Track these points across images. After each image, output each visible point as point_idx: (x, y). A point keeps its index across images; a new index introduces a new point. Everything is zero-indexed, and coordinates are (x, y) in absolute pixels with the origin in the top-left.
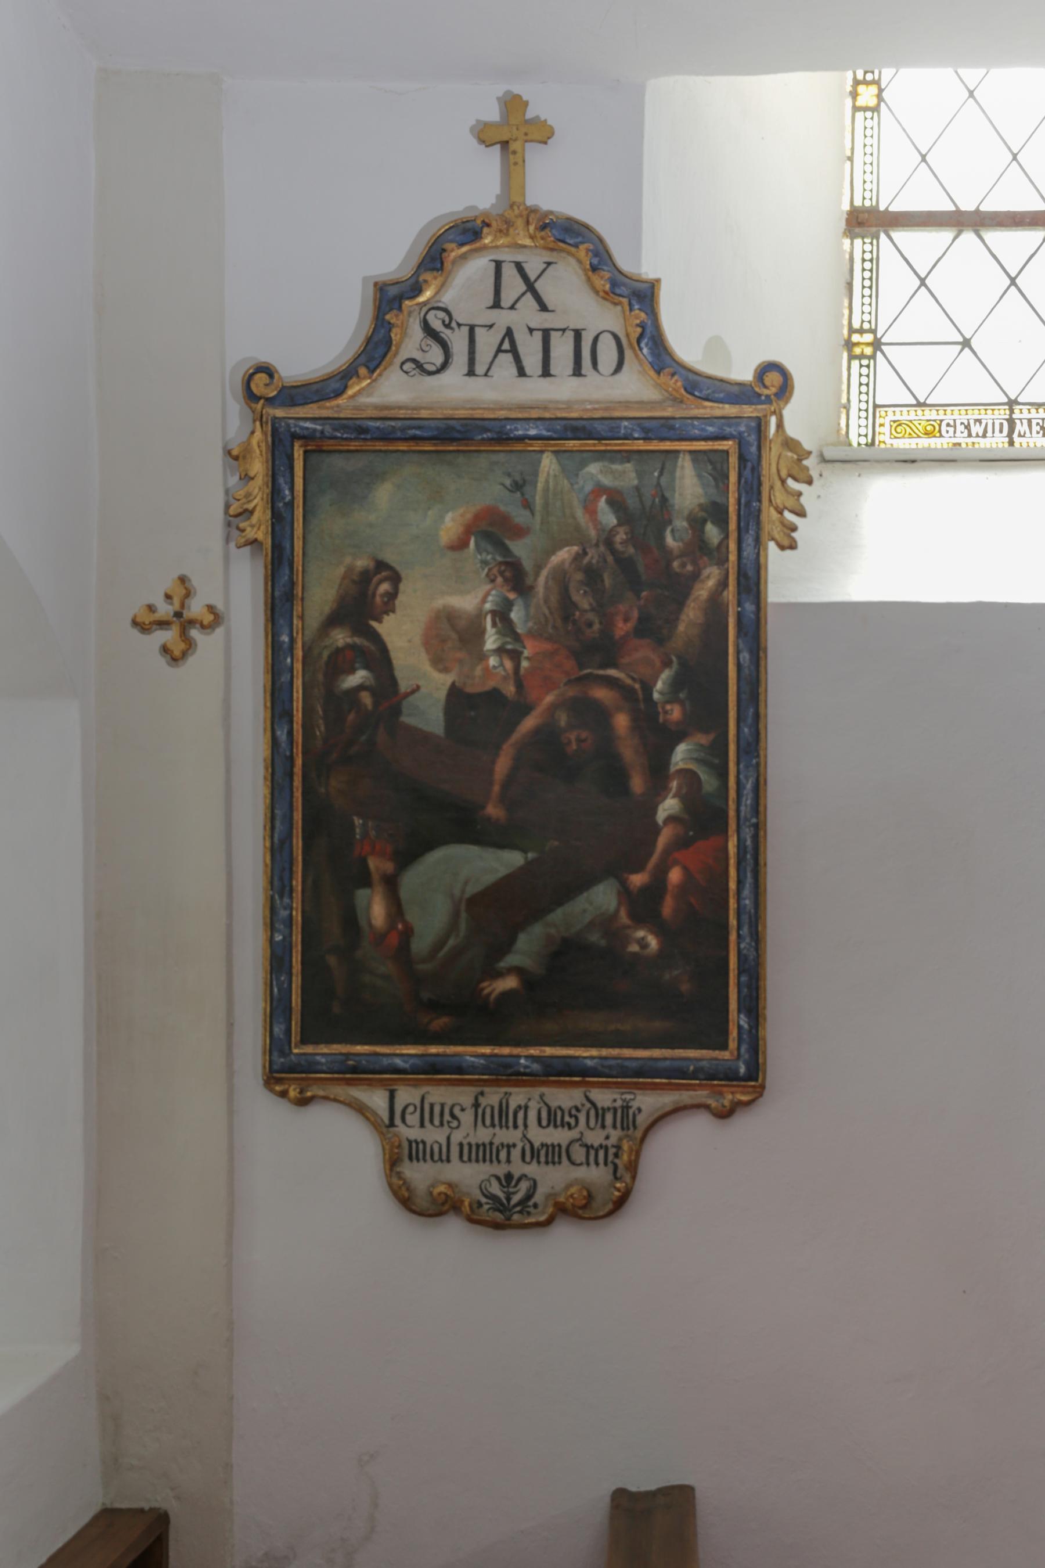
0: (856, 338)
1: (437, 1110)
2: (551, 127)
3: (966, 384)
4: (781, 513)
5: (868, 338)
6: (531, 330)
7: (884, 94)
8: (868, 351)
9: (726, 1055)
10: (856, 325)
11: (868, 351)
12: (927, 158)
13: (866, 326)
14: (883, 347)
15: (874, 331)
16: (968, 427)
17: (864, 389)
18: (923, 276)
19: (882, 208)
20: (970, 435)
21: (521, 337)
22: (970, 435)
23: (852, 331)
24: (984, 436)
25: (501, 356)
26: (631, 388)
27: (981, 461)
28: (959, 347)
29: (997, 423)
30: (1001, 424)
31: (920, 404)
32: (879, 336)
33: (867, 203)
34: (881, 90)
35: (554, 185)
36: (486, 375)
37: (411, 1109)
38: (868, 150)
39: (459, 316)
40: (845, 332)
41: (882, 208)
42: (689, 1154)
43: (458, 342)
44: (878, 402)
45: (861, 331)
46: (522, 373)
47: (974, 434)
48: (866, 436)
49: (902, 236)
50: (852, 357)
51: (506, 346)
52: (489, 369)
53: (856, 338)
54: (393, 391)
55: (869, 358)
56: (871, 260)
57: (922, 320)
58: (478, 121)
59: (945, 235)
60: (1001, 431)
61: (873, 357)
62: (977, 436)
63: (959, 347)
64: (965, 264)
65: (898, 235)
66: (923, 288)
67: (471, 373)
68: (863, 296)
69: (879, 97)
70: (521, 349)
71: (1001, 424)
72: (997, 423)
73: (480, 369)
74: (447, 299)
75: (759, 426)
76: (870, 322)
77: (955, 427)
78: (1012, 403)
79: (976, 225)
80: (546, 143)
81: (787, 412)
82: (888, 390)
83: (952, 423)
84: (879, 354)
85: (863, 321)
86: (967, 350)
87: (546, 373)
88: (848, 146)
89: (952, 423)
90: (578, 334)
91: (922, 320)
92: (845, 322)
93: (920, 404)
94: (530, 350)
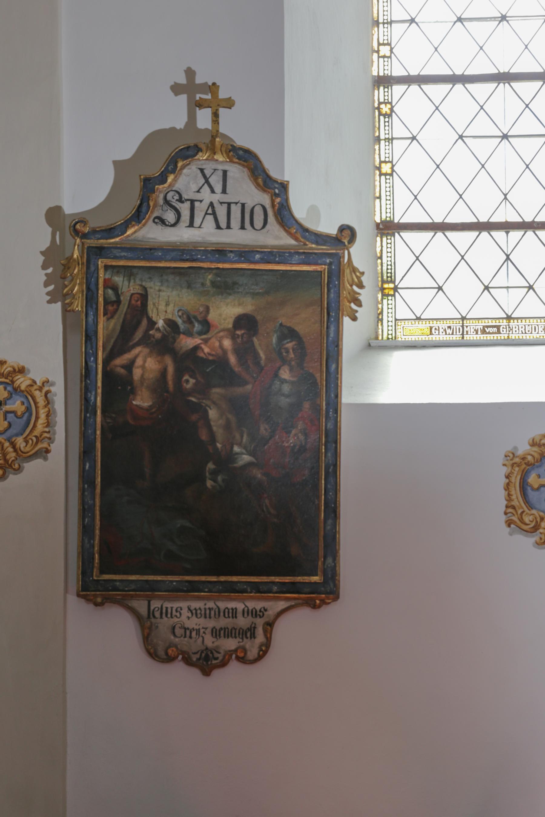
0: (386, 286)
1: (169, 611)
2: (234, 101)
3: (441, 308)
4: (351, 286)
5: (391, 285)
6: (221, 203)
7: (395, 168)
8: (392, 292)
9: (315, 579)
10: (381, 42)
11: (392, 292)
12: (417, 197)
13: (387, 160)
14: (399, 290)
15: (394, 282)
16: (445, 330)
17: (387, 124)
18: (417, 261)
19: (396, 221)
20: (446, 334)
21: (216, 205)
22: (446, 334)
23: (383, 282)
24: (453, 334)
25: (207, 216)
26: (275, 237)
27: (435, 22)
28: (490, 290)
29: (458, 328)
30: (459, 328)
31: (418, 319)
32: (396, 284)
33: (388, 219)
34: (393, 166)
35: (235, 127)
36: (200, 227)
37: (157, 609)
38: (390, 306)
39: (185, 196)
40: (380, 284)
41: (396, 221)
42: (297, 629)
43: (185, 209)
44: (397, 318)
45: (388, 282)
46: (218, 227)
47: (448, 333)
48: (389, 157)
49: (406, 235)
50: (383, 295)
51: (210, 211)
52: (201, 225)
53: (386, 286)
54: (151, 233)
55: (392, 295)
56: (390, 187)
57: (417, 277)
58: (175, 83)
59: (445, 87)
60: (459, 332)
61: (394, 295)
62: (449, 334)
63: (437, 290)
64: (439, 250)
65: (404, 234)
66: (417, 261)
67: (191, 225)
68: (386, 191)
69: (392, 168)
70: (217, 213)
71: (459, 328)
72: (458, 328)
73: (197, 221)
74: (179, 185)
75: (338, 258)
76: (388, 40)
77: (439, 330)
78: (463, 318)
79: (443, 230)
80: (230, 108)
81: (351, 250)
82: (403, 312)
83: (437, 328)
84: (396, 293)
85: (384, 40)
86: (440, 291)
87: (229, 227)
88: (377, 190)
89: (437, 328)
90: (243, 205)
91: (417, 277)
92: (380, 279)
93: (418, 319)
94: (221, 212)
